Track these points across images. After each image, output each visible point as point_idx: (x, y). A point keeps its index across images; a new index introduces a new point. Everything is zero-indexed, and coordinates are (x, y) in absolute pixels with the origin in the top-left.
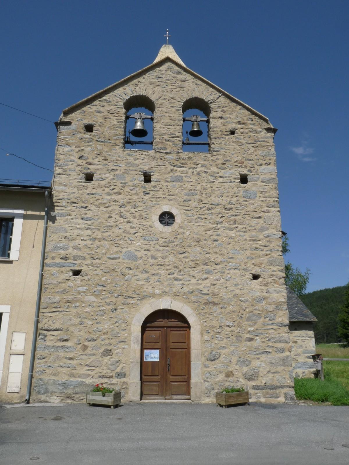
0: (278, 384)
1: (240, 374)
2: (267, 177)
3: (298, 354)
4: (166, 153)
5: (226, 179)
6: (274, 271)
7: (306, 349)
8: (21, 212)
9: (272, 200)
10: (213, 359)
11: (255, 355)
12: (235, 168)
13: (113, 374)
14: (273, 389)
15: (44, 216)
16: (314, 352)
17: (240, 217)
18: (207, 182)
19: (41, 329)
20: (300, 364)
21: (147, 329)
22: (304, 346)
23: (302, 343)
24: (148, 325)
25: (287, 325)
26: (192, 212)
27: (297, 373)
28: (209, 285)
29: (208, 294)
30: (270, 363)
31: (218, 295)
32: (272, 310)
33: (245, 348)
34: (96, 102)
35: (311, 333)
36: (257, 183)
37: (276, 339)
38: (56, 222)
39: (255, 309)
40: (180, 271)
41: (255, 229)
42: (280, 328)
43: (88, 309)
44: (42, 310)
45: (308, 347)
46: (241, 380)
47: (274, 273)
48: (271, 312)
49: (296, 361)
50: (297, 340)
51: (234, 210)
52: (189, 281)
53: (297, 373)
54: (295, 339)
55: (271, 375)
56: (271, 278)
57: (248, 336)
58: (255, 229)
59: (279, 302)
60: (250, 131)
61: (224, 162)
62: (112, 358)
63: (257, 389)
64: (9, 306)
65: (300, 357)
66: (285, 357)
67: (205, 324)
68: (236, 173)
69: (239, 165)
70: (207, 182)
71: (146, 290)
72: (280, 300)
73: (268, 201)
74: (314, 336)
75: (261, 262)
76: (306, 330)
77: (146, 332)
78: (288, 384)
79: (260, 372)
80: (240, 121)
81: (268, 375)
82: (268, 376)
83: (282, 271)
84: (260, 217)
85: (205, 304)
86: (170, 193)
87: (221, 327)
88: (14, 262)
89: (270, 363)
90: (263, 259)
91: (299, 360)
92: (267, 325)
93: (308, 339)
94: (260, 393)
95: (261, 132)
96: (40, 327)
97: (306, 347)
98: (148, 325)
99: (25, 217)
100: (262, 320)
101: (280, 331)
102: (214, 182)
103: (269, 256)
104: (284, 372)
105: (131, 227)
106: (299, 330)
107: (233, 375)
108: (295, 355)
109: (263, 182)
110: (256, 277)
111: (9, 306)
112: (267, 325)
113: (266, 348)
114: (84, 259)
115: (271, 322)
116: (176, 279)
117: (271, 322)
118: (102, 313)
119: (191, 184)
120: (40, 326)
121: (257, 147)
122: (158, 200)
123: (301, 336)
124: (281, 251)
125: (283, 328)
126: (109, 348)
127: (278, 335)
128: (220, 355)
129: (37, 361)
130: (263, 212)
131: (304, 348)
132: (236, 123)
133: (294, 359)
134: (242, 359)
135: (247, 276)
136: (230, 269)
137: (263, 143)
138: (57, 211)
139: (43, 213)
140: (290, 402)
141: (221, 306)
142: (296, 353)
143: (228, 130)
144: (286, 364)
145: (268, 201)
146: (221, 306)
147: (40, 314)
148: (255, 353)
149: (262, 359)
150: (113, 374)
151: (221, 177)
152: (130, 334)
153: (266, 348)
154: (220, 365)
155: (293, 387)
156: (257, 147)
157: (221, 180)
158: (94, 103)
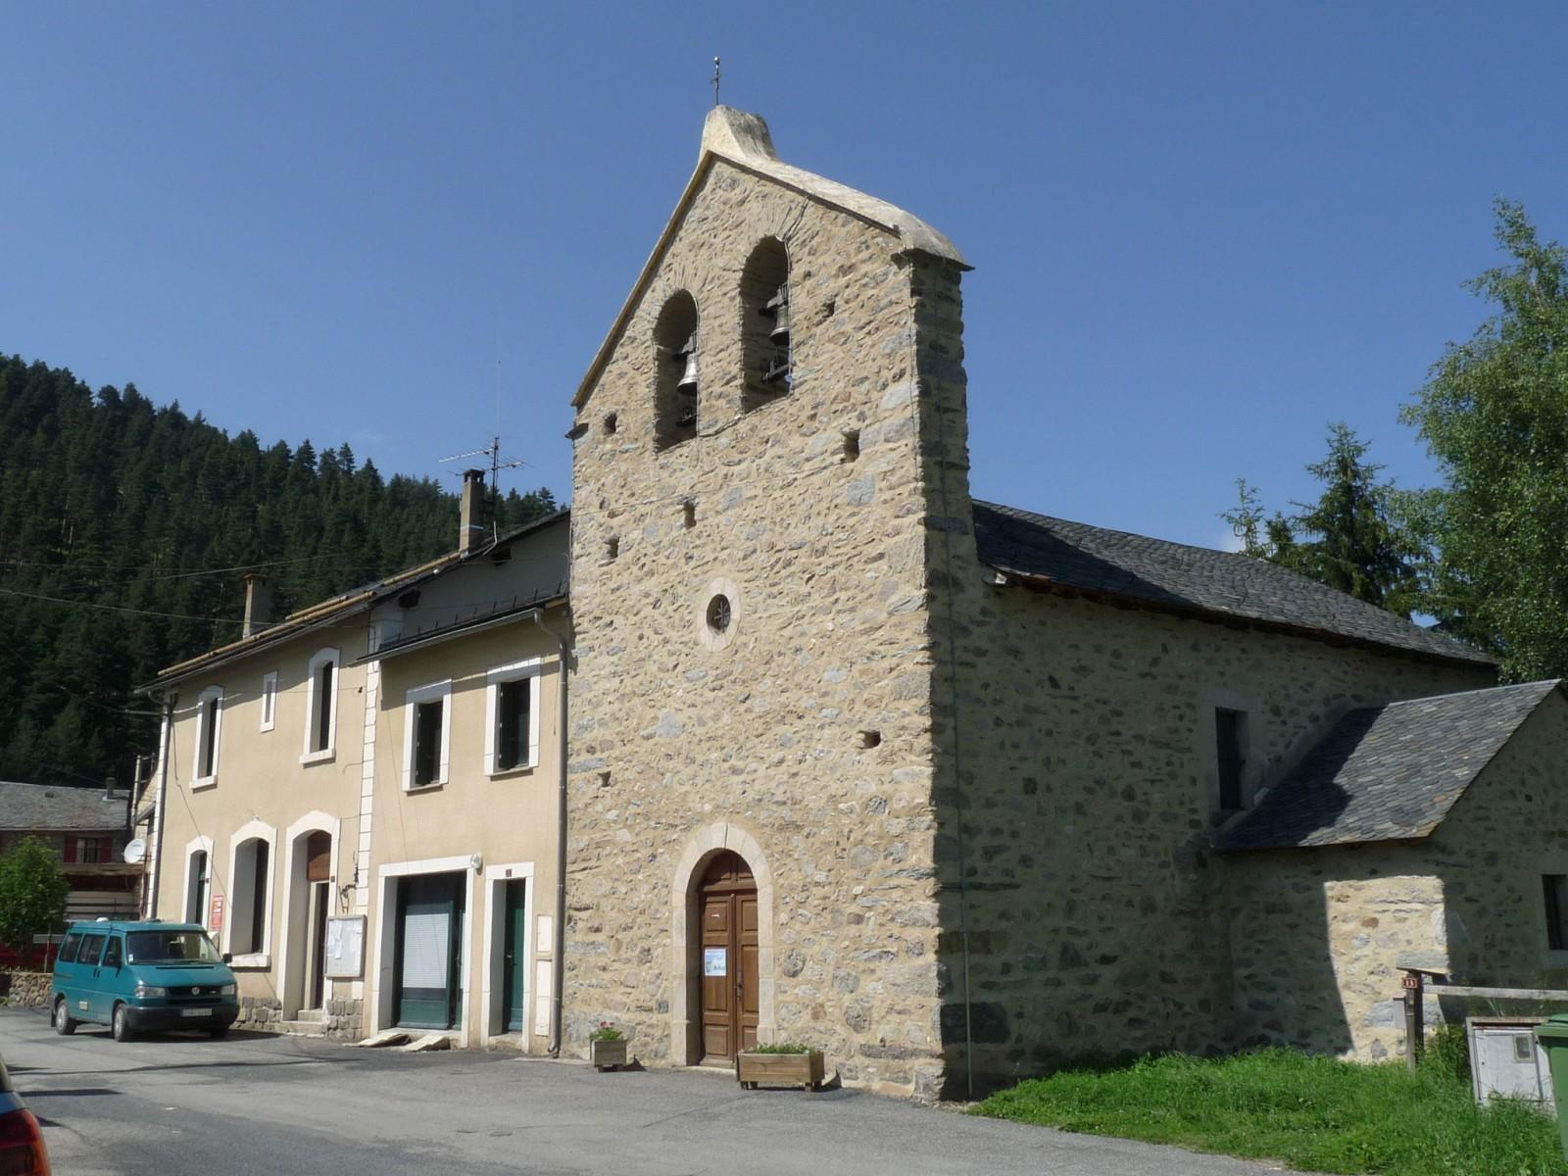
0: (909, 1046)
1: (837, 1012)
2: (896, 422)
3: (1381, 969)
4: (717, 433)
5: (816, 463)
6: (905, 715)
7: (1409, 949)
8: (536, 661)
9: (905, 490)
10: (792, 970)
11: (866, 960)
12: (835, 419)
13: (653, 1004)
14: (897, 1057)
15: (558, 662)
16: (1441, 961)
17: (840, 569)
18: (782, 488)
19: (570, 908)
20: (1387, 1006)
21: (709, 899)
22: (1401, 936)
23: (1398, 926)
24: (707, 888)
25: (928, 876)
26: (758, 583)
27: (1377, 1040)
28: (785, 777)
29: (784, 803)
30: (894, 985)
31: (801, 801)
32: (899, 831)
33: (847, 943)
34: (618, 352)
35: (1430, 885)
36: (876, 448)
37: (906, 917)
38: (578, 669)
39: (867, 834)
40: (740, 748)
41: (871, 596)
42: (915, 882)
43: (620, 861)
44: (569, 868)
45: (1414, 943)
46: (838, 1028)
47: (906, 721)
48: (898, 839)
49: (1373, 996)
50: (1377, 916)
51: (832, 551)
52: (755, 771)
53: (1377, 1040)
54: (1371, 911)
55: (894, 1018)
56: (900, 736)
57: (854, 909)
58: (871, 596)
59: (914, 808)
60: (865, 285)
61: (813, 412)
62: (650, 968)
63: (869, 1056)
64: (532, 864)
65: (1388, 980)
66: (922, 967)
67: (781, 881)
68: (831, 437)
69: (841, 407)
70: (782, 488)
71: (691, 805)
72: (917, 801)
73: (897, 498)
74: (1440, 897)
75: (880, 692)
76: (1410, 874)
77: (708, 906)
78: (928, 1048)
79: (874, 1010)
80: (842, 266)
81: (889, 1017)
82: (889, 1022)
83: (921, 713)
84: (881, 556)
85: (781, 829)
86: (724, 544)
87: (805, 888)
88: (535, 770)
89: (894, 985)
90: (886, 681)
91: (1383, 992)
92: (891, 876)
93: (1417, 911)
94: (873, 1066)
95: (886, 274)
96: (567, 903)
97: (1409, 942)
98: (707, 888)
99: (455, 689)
100: (880, 862)
101: (915, 892)
102: (795, 479)
103: (895, 673)
104: (921, 1012)
105: (671, 654)
106: (1384, 876)
107: (825, 1013)
108: (1372, 973)
109: (887, 441)
110: (873, 739)
111: (532, 864)
112: (891, 876)
113: (885, 942)
114: (611, 745)
115: (897, 867)
116: (735, 771)
117: (897, 867)
118: (635, 866)
119: (756, 502)
120: (569, 900)
121: (877, 329)
122: (706, 568)
123: (1391, 899)
124: (923, 649)
125: (923, 881)
126: (645, 944)
127: (909, 905)
128: (804, 962)
129: (567, 974)
130: (888, 535)
131: (1403, 946)
132: (837, 276)
133: (1368, 985)
134: (841, 973)
135: (853, 740)
136: (822, 727)
137: (891, 309)
138: (580, 645)
139: (556, 657)
140: (922, 1095)
141: (806, 831)
142: (1375, 964)
143: (819, 307)
144: (924, 988)
145: (897, 498)
146: (806, 831)
147: (568, 876)
148: (865, 956)
149: (879, 973)
150: (653, 1004)
151: (808, 460)
152: (671, 912)
153: (885, 942)
154: (803, 987)
155: (940, 1056)
156: (877, 329)
157: (808, 466)
158: (615, 356)
